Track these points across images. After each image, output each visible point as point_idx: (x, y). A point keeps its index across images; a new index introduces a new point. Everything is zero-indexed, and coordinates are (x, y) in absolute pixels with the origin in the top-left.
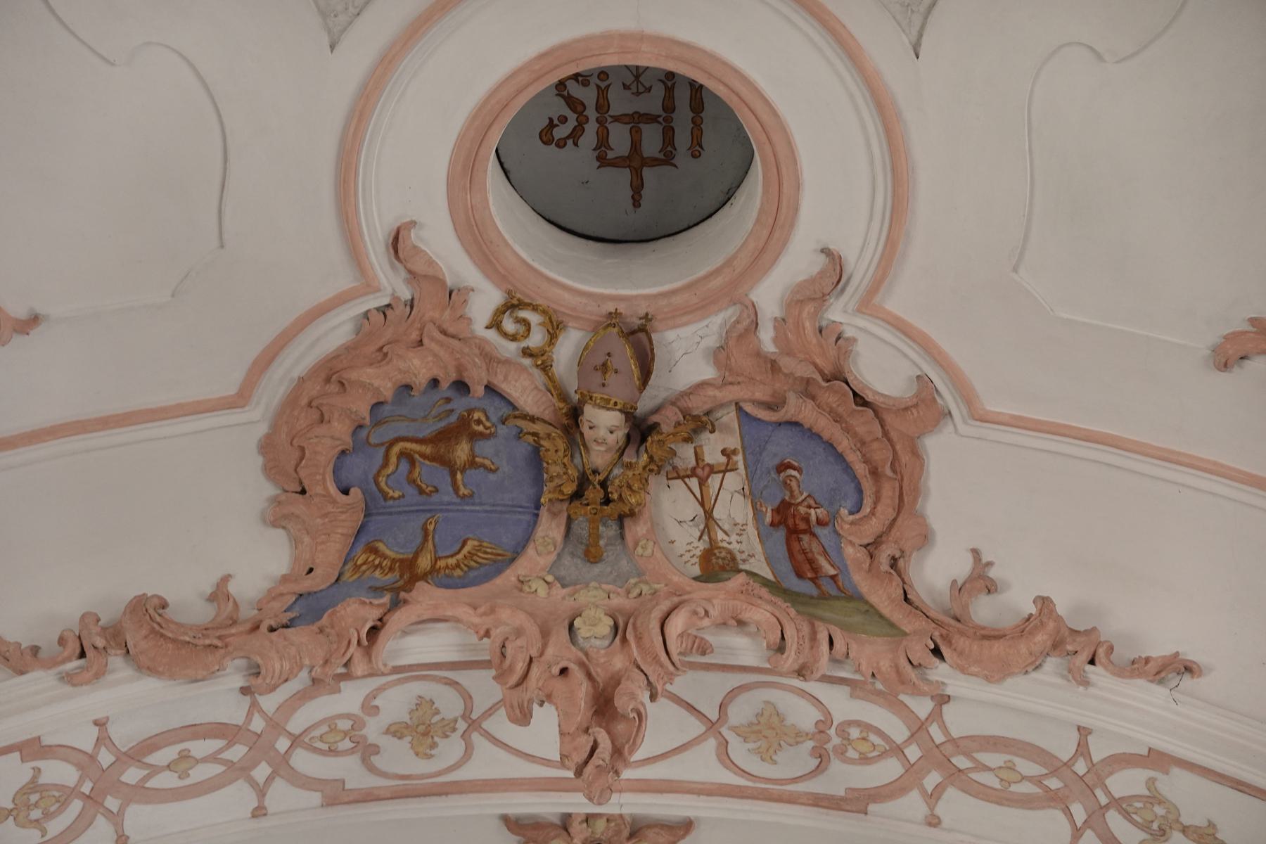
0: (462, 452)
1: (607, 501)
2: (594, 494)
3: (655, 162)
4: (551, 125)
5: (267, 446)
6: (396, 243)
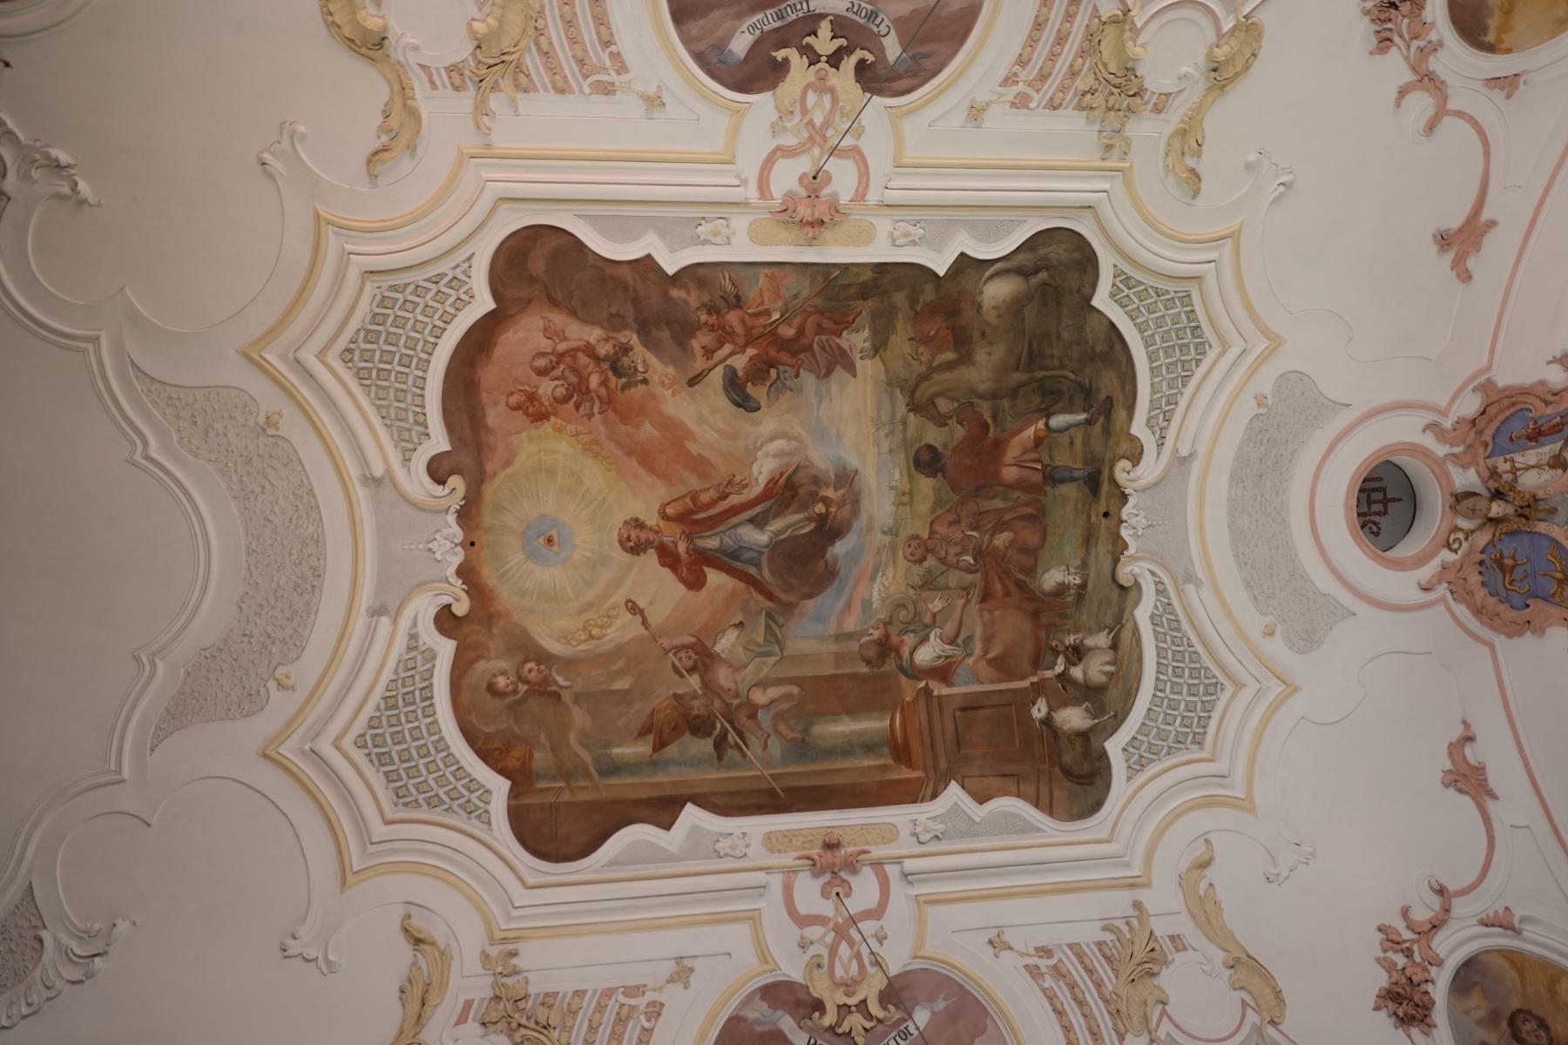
0: (1508, 562)
1: (1529, 506)
2: (1526, 511)
3: (1385, 493)
4: (1373, 532)
5: (1510, 635)
6: (1426, 590)
